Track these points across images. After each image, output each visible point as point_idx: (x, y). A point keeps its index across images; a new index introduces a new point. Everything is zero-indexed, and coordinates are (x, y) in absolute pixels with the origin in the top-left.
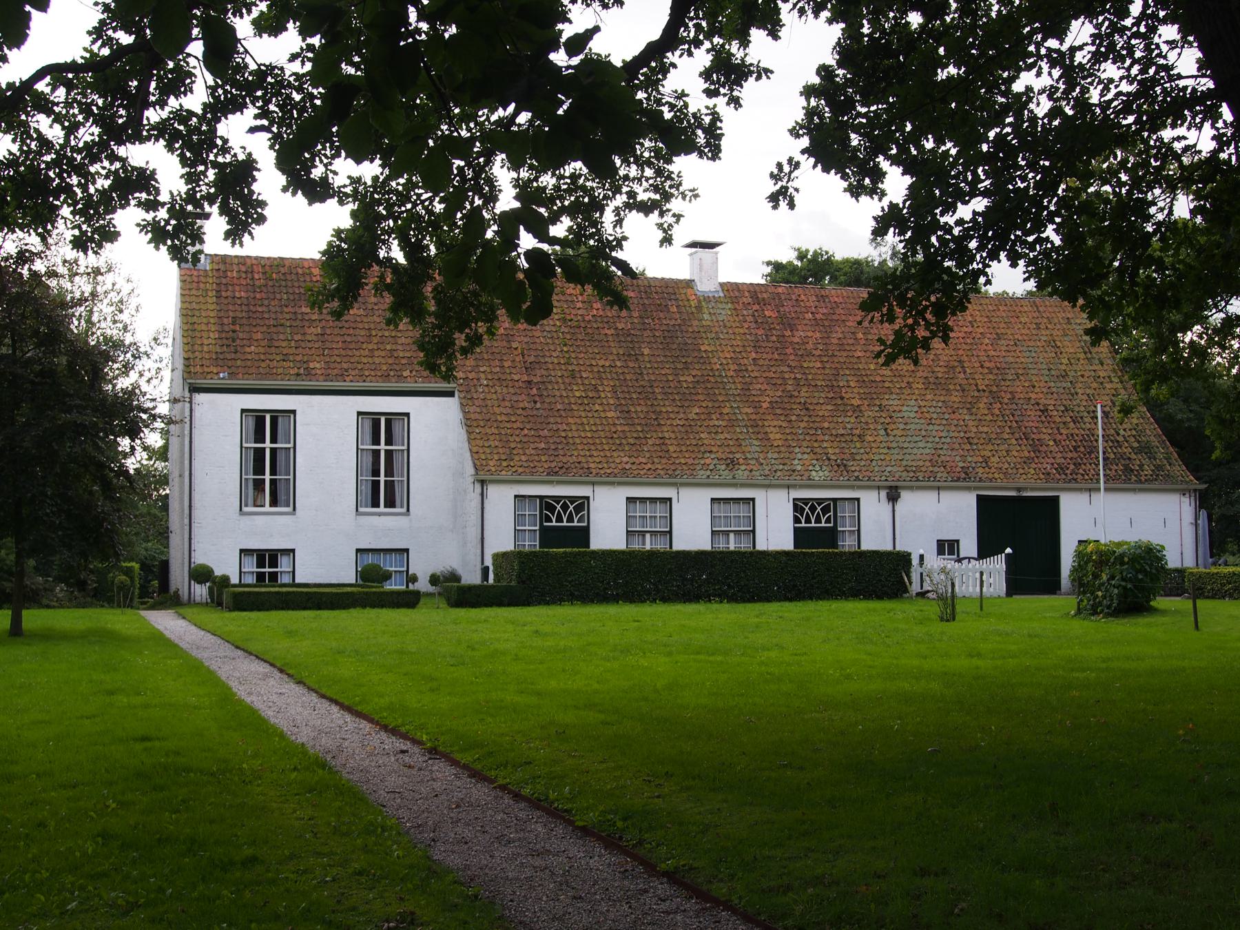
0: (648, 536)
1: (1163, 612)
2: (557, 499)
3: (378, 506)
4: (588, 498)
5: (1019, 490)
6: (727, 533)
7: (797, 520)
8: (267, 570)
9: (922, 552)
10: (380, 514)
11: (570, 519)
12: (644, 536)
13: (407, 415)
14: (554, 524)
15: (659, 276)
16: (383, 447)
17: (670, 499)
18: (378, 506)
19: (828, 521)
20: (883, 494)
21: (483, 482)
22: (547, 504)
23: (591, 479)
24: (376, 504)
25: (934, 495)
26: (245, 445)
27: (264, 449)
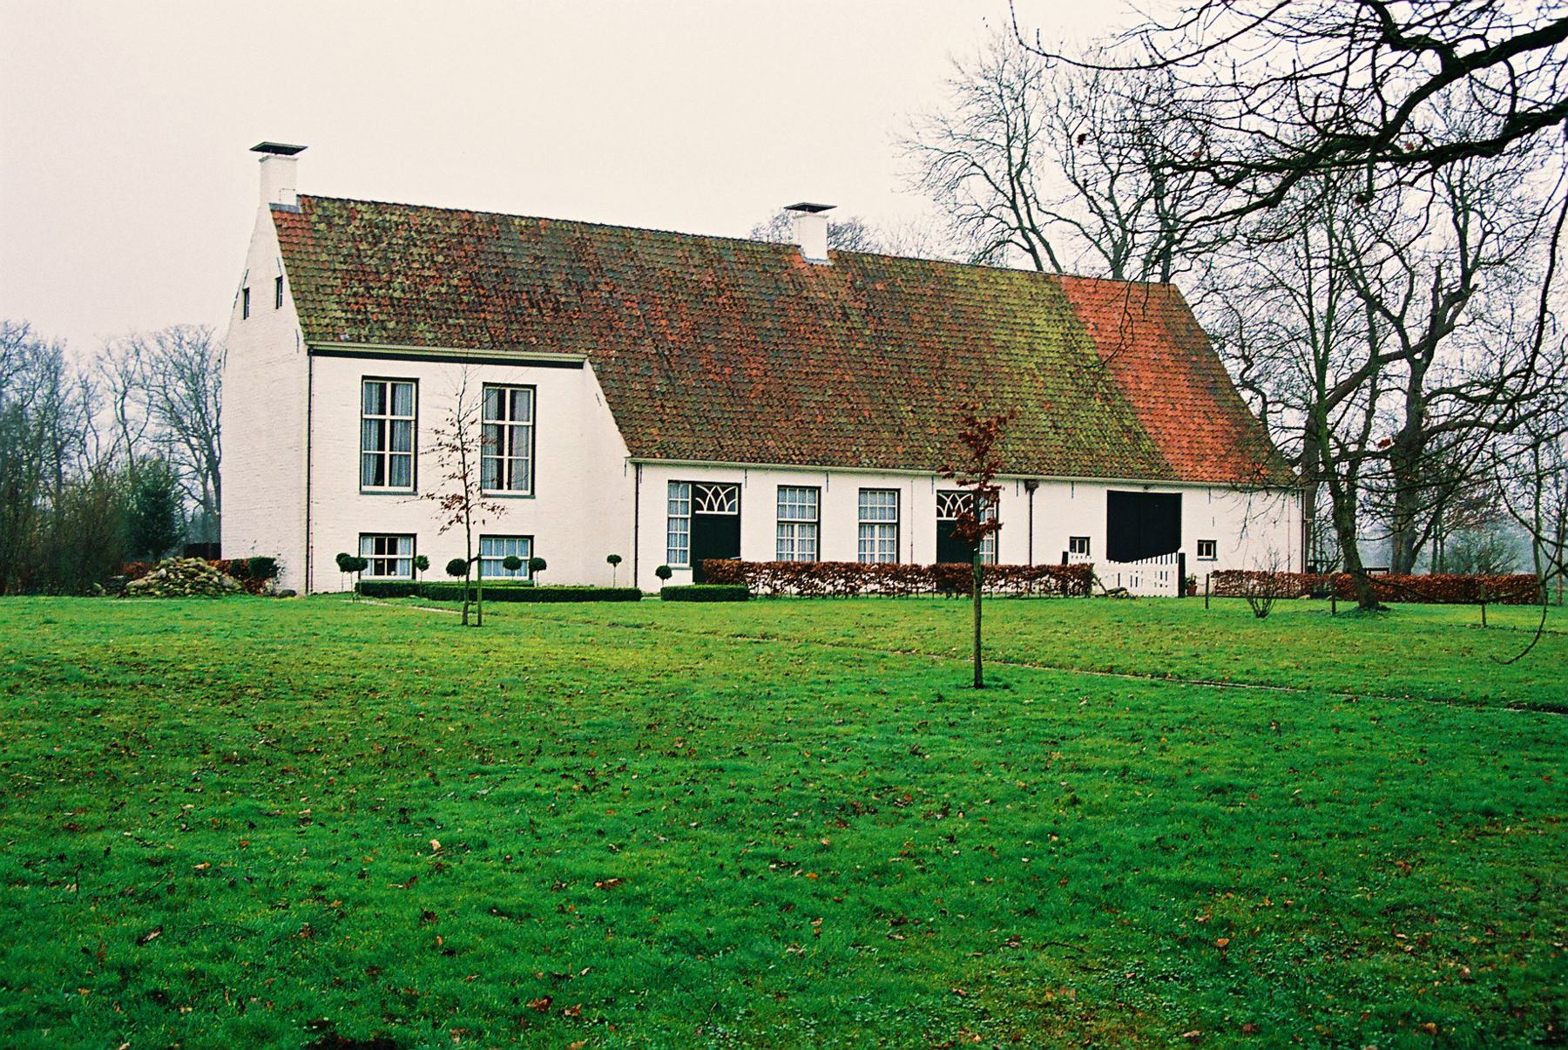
0: (796, 526)
2: (709, 485)
3: (383, 484)
4: (739, 485)
5: (1146, 486)
6: (872, 525)
7: (939, 514)
8: (386, 556)
11: (721, 508)
12: (873, 528)
13: (534, 387)
14: (705, 512)
17: (819, 488)
18: (383, 484)
20: (1022, 486)
21: (638, 466)
22: (698, 490)
23: (824, 468)
24: (379, 480)
25: (1205, 493)
26: (365, 416)
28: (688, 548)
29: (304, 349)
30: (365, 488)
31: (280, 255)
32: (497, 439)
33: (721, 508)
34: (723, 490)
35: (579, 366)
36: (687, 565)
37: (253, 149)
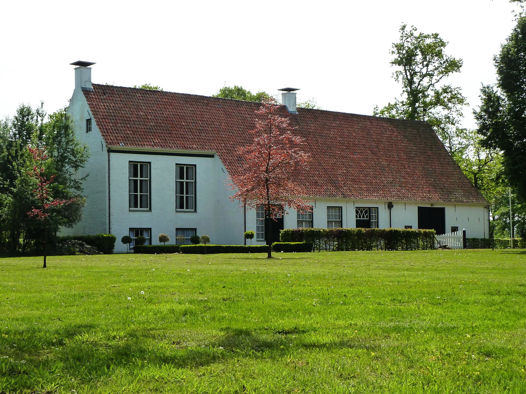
0: (304, 223)
1: (275, 258)
7: (357, 217)
9: (464, 229)
10: (185, 212)
11: (363, 217)
15: (194, 94)
16: (139, 178)
18: (184, 209)
19: (367, 217)
24: (136, 206)
27: (137, 180)
28: (264, 232)
29: (105, 149)
30: (178, 210)
31: (89, 109)
32: (181, 188)
33: (363, 217)
34: (364, 210)
35: (212, 156)
36: (264, 239)
37: (71, 64)
